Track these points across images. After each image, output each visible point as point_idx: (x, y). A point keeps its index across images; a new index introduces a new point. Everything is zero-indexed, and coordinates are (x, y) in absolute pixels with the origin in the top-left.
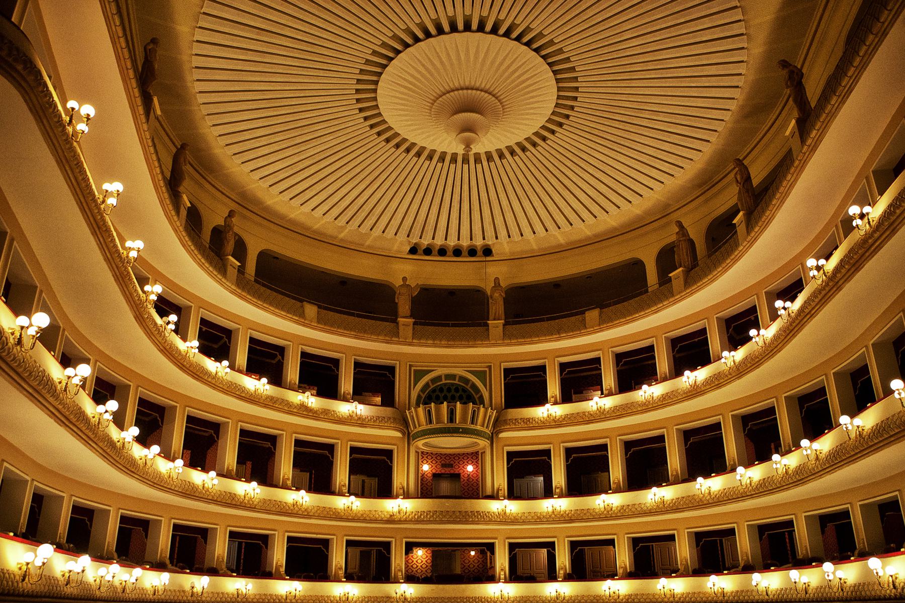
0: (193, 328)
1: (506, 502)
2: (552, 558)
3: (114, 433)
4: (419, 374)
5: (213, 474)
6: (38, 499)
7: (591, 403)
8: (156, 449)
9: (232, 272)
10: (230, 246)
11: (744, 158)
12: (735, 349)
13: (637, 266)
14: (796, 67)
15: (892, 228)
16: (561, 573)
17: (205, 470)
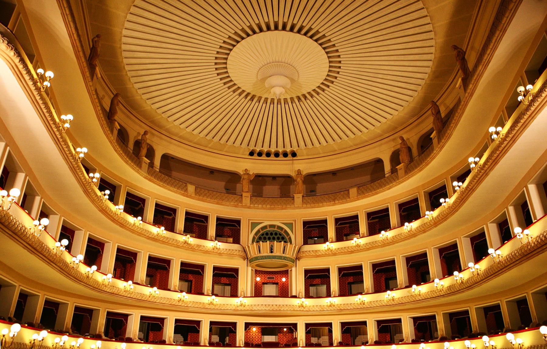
0: (122, 198)
1: (303, 299)
2: (330, 331)
3: (68, 258)
4: (254, 225)
5: (130, 282)
6: (24, 296)
7: (352, 241)
8: (94, 268)
9: (145, 166)
10: (144, 151)
11: (437, 101)
12: (433, 210)
13: (379, 162)
14: (461, 49)
15: (513, 139)
16: (335, 343)
17: (126, 280)
